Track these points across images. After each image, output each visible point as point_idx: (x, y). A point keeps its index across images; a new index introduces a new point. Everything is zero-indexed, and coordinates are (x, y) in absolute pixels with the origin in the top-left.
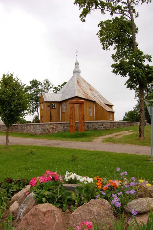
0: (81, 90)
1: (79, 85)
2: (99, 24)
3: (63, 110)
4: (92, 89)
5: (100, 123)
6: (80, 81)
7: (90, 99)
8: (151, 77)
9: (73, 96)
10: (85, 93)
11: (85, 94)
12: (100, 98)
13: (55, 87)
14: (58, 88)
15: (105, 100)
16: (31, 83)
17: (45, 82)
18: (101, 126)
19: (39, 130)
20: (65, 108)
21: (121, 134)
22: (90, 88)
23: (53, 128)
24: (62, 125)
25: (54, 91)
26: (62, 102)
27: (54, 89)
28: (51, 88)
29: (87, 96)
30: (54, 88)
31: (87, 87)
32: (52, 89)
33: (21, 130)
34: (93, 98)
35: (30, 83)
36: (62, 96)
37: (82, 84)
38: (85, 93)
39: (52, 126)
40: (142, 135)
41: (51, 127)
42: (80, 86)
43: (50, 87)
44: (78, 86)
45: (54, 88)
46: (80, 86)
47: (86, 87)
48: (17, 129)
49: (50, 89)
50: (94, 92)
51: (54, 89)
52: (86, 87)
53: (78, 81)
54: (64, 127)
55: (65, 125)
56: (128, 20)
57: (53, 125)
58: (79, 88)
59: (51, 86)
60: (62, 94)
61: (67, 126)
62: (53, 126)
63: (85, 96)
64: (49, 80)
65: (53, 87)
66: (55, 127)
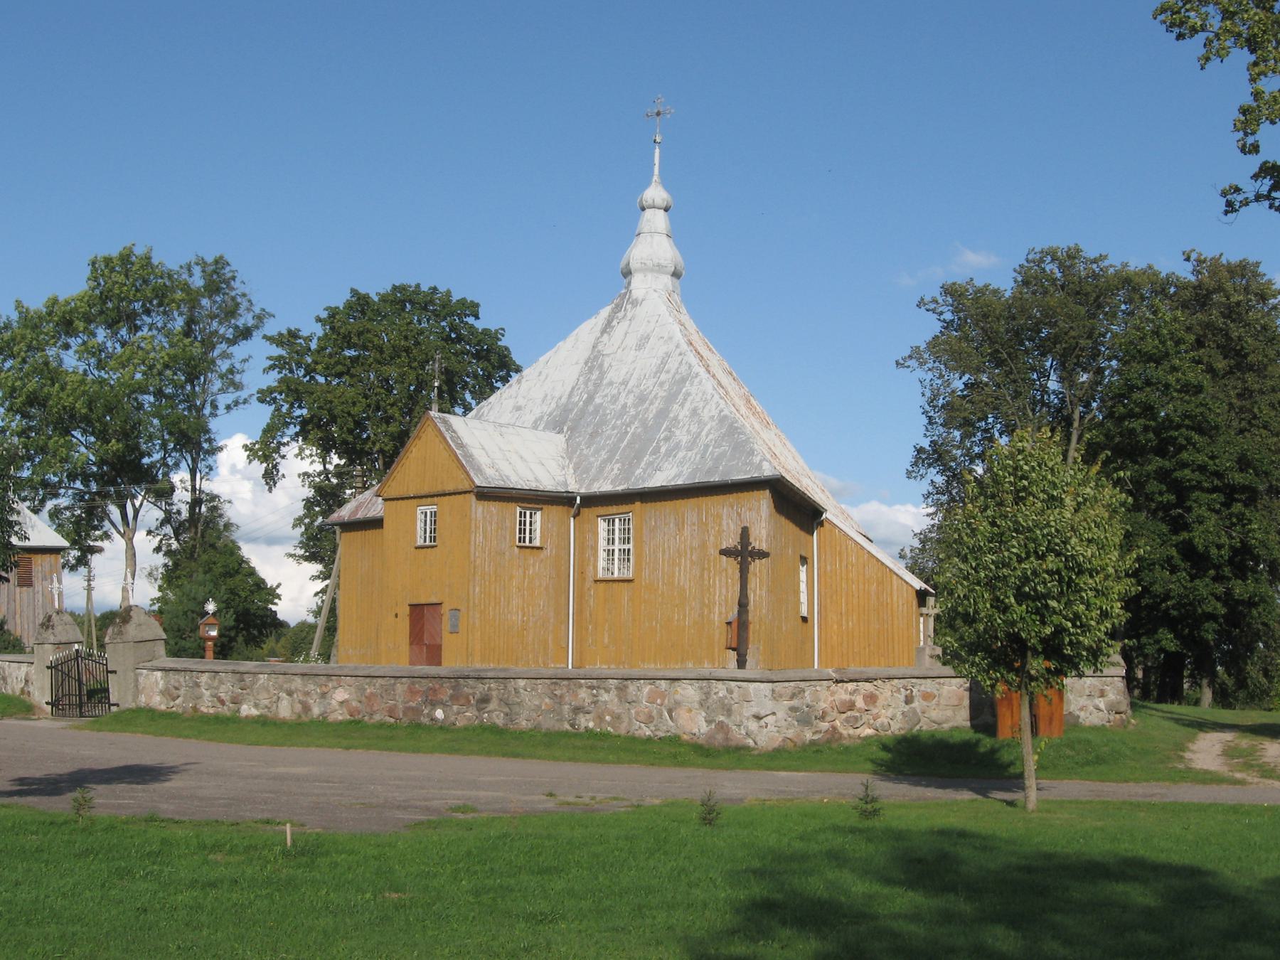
3: (602, 563)
23: (851, 706)
24: (898, 691)
28: (246, 334)
41: (843, 703)
45: (278, 340)
54: (909, 700)
57: (851, 686)
59: (245, 319)
62: (855, 691)
65: (272, 328)
66: (860, 703)
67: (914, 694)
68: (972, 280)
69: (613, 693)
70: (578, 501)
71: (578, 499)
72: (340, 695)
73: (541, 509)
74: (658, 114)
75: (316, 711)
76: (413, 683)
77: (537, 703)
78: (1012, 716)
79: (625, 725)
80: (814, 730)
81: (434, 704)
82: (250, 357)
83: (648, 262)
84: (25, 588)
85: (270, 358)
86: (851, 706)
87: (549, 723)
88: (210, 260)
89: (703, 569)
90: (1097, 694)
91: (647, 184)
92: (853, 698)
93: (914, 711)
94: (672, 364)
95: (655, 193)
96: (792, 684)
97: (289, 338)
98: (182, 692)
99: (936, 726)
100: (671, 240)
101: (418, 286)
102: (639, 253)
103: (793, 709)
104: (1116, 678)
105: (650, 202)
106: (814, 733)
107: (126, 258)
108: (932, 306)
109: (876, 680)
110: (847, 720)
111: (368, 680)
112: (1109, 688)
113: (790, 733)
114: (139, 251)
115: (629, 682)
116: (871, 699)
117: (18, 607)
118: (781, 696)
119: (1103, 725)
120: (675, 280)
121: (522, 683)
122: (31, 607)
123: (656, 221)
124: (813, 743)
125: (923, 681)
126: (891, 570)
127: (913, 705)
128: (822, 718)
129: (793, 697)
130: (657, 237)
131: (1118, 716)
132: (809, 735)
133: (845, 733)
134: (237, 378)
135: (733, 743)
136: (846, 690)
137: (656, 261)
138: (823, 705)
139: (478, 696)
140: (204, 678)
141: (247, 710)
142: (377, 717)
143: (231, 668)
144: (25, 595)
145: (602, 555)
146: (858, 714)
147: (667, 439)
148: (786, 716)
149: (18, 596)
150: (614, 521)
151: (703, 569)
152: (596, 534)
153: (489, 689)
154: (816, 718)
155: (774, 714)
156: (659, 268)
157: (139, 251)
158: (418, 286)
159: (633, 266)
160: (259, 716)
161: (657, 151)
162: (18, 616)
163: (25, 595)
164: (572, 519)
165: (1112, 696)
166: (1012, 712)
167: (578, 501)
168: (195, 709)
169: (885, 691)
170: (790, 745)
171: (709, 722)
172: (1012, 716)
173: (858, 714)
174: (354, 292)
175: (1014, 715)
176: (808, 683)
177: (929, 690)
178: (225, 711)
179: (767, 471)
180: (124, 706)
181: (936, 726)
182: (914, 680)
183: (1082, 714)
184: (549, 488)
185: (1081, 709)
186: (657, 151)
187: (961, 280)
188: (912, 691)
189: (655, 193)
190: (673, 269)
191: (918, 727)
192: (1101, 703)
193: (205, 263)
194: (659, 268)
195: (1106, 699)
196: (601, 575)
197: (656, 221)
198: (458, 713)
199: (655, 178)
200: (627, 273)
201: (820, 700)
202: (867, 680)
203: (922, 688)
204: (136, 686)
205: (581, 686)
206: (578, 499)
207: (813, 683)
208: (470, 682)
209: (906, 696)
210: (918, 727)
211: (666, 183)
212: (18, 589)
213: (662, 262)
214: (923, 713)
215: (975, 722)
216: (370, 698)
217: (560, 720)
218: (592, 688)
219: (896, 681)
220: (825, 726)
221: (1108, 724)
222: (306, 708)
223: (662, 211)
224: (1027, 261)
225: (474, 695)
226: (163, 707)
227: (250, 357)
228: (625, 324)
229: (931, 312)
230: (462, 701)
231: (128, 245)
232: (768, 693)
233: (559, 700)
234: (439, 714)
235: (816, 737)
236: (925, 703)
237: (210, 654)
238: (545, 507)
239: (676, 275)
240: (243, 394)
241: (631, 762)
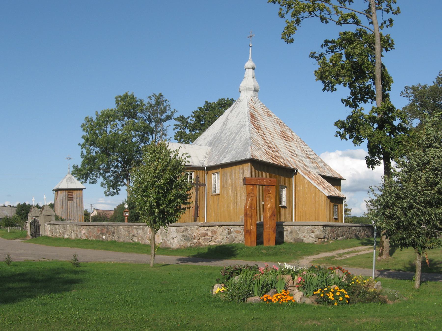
0: (261, 141)
1: (254, 126)
2: (321, 21)
3: (213, 189)
4: (287, 136)
5: (307, 227)
6: (257, 115)
7: (283, 164)
8: (440, 104)
9: (242, 159)
10: (271, 149)
11: (271, 151)
12: (309, 158)
13: (182, 118)
14: (191, 118)
15: (320, 164)
16: (117, 103)
17: (153, 102)
18: (310, 234)
19: (176, 239)
20: (219, 183)
21: (355, 252)
22: (283, 133)
23: (206, 235)
24: (225, 230)
25: (176, 126)
26: (210, 168)
27: (179, 123)
28: (168, 118)
29: (276, 155)
30: (177, 119)
31: (275, 130)
32: (172, 123)
33: (129, 237)
34: (290, 159)
35: (117, 100)
36: (210, 153)
37: (262, 124)
38: (271, 149)
39: (204, 232)
40: (384, 252)
41: (202, 234)
42: (259, 129)
43: (165, 115)
44: (254, 130)
45: (177, 119)
46: (259, 129)
47: (272, 130)
48: (115, 234)
49: (165, 120)
50: (292, 144)
51: (179, 123)
52: (272, 130)
53: (253, 116)
54: (229, 233)
55: (232, 230)
56: (366, 138)
57: (206, 228)
58: (256, 136)
59: (169, 113)
60: (210, 148)
61: (237, 232)
62: (207, 230)
63: (272, 156)
64: (166, 96)
65: (176, 115)
66: (210, 234)
67: (231, 231)
68: (420, 84)
69: (141, 230)
70: (205, 169)
71: (206, 168)
72: (84, 231)
73: (194, 172)
74: (251, 37)
75: (79, 236)
76: (98, 228)
77: (124, 233)
78: (251, 239)
79: (144, 240)
80: (191, 242)
81: (103, 234)
82: (170, 125)
83: (245, 87)
84: (71, 201)
85: (175, 125)
86: (206, 235)
87: (127, 240)
88: (158, 95)
89: (235, 191)
90: (311, 231)
91: (247, 61)
92: (207, 232)
93: (232, 236)
94: (241, 122)
95: (250, 64)
96: (183, 227)
97: (182, 119)
98: (54, 231)
99: (241, 242)
100: (255, 80)
101: (228, 99)
102: (243, 85)
103: (183, 235)
104: (319, 226)
105: (247, 67)
106: (191, 244)
107: (126, 96)
108: (406, 94)
109: (216, 226)
110: (204, 239)
111: (89, 227)
112: (316, 230)
113: (182, 243)
114: (129, 94)
115: (145, 227)
116: (214, 232)
117: (68, 207)
118: (179, 231)
119: (313, 243)
120: (255, 92)
121: (121, 227)
122: (73, 207)
123: (250, 73)
124: (191, 247)
125: (235, 226)
126: (318, 189)
127: (232, 235)
128: (194, 238)
129: (183, 231)
130: (249, 78)
131: (320, 240)
132: (189, 244)
133: (203, 244)
134: (165, 132)
135: (167, 247)
136: (204, 230)
137: (247, 87)
138: (194, 234)
139: (112, 231)
140: (57, 226)
141: (66, 236)
142: (91, 238)
143: (62, 223)
144: (71, 203)
145: (213, 186)
146: (209, 238)
147: (231, 147)
148: (180, 238)
149: (68, 204)
150: (192, 173)
151: (235, 191)
152: (211, 179)
153: (115, 229)
154: (192, 238)
155: (177, 237)
156: (248, 89)
157: (129, 94)
158: (228, 99)
159: (241, 89)
160: (67, 238)
161: (250, 49)
162: (68, 210)
163: (71, 203)
164: (206, 175)
165: (318, 232)
166: (251, 237)
167: (205, 169)
168: (56, 236)
169: (220, 230)
170: (182, 247)
171: (162, 239)
172: (251, 239)
173: (209, 238)
174: (207, 102)
175: (252, 238)
176: (189, 227)
177: (238, 230)
178: (61, 236)
179: (249, 156)
180: (43, 235)
181: (241, 242)
182: (231, 226)
183: (305, 239)
184: (196, 165)
185: (304, 237)
186: (250, 49)
187: (416, 85)
188: (231, 230)
189: (250, 64)
190: (254, 89)
191: (234, 242)
192: (313, 235)
193: (156, 96)
194: (248, 89)
195: (315, 233)
196: (213, 193)
197: (250, 73)
198: (108, 237)
199: (250, 58)
200: (240, 92)
201: (193, 233)
202: (212, 226)
203: (235, 229)
204: (45, 229)
205: (134, 228)
206: (206, 168)
207: (191, 227)
208: (110, 227)
209: (228, 232)
210: (234, 242)
211: (253, 60)
212: (68, 201)
213: (250, 87)
214: (236, 237)
215: (258, 241)
216: (90, 232)
217: (129, 239)
218: (137, 229)
219: (224, 226)
220: (195, 241)
221: (315, 242)
222: (77, 236)
223: (251, 69)
224: (439, 75)
225: (111, 231)
226: (50, 236)
227: (170, 125)
228: (236, 109)
229: (405, 97)
230: (109, 233)
231: (127, 92)
232: (175, 230)
233: (129, 232)
234: (104, 237)
235: (192, 245)
236: (237, 234)
237: (126, 221)
238: (195, 171)
239: (255, 90)
240: (168, 137)
241: (131, 252)
